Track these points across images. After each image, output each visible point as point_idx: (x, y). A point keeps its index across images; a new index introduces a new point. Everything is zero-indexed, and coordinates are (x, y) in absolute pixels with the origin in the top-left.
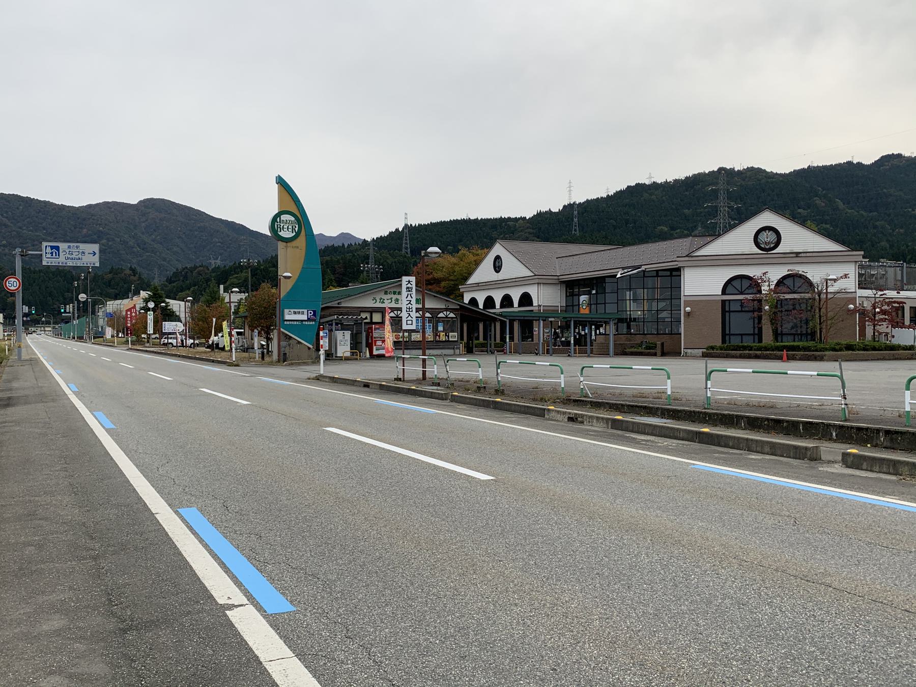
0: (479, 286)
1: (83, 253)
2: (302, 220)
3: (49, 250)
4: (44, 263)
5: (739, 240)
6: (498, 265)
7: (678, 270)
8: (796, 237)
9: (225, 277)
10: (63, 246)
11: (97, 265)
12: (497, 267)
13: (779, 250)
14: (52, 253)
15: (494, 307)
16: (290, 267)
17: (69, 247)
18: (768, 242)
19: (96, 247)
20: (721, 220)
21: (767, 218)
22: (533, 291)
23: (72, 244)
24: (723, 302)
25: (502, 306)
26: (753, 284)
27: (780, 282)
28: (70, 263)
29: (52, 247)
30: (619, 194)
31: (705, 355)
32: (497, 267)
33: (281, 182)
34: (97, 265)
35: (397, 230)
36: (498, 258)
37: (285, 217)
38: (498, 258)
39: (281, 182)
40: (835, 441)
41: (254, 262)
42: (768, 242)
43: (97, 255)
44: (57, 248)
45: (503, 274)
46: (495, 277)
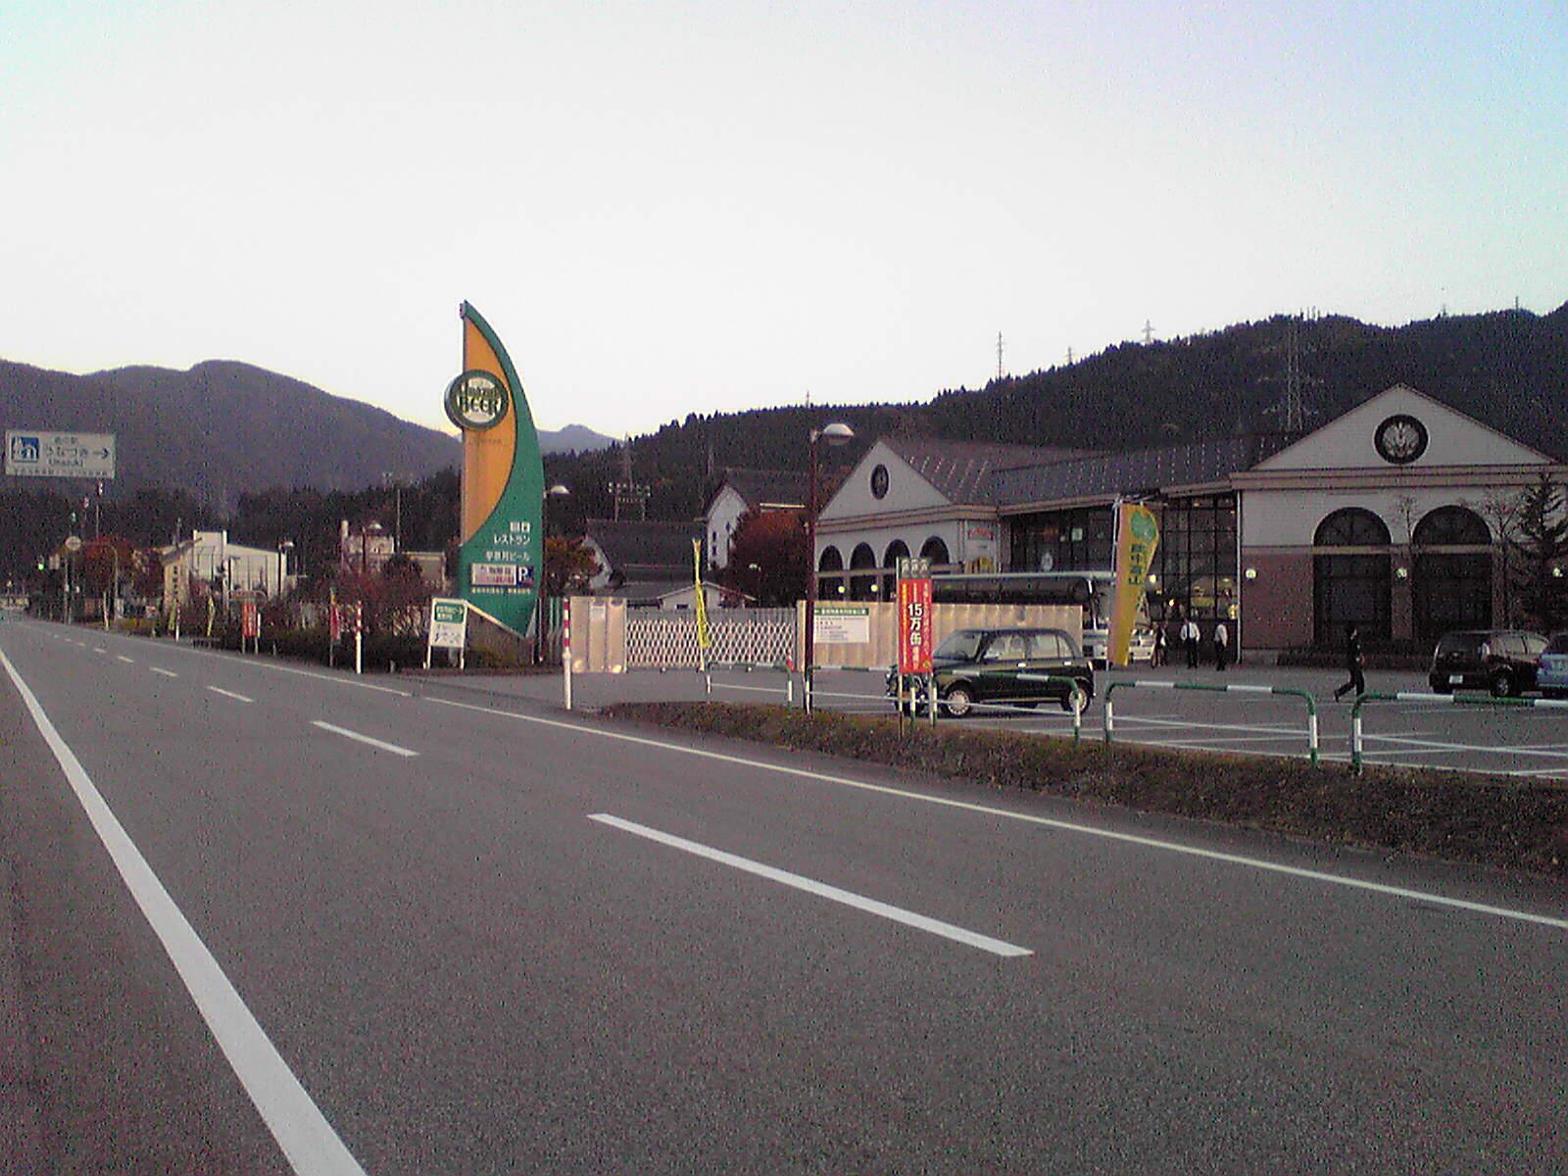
0: (848, 525)
1: (85, 452)
2: (508, 392)
3: (18, 444)
4: (9, 471)
5: (1347, 441)
6: (879, 484)
7: (1232, 495)
8: (1456, 439)
9: (361, 507)
10: (45, 438)
11: (112, 475)
12: (879, 487)
13: (1420, 461)
14: (24, 453)
15: (839, 565)
16: (485, 483)
17: (57, 440)
18: (1401, 450)
19: (109, 442)
20: (1292, 409)
21: (1399, 400)
22: (949, 535)
23: (62, 436)
24: (1317, 559)
25: (854, 565)
26: (1368, 525)
27: (1426, 522)
28: (58, 472)
29: (25, 441)
30: (1093, 361)
31: (1284, 662)
32: (879, 487)
33: (469, 314)
34: (112, 475)
35: (675, 423)
36: (880, 471)
37: (474, 383)
38: (880, 471)
39: (469, 314)
40: (463, 673)
41: (412, 479)
42: (1401, 450)
43: (111, 459)
44: (35, 443)
45: (892, 501)
46: (874, 506)
